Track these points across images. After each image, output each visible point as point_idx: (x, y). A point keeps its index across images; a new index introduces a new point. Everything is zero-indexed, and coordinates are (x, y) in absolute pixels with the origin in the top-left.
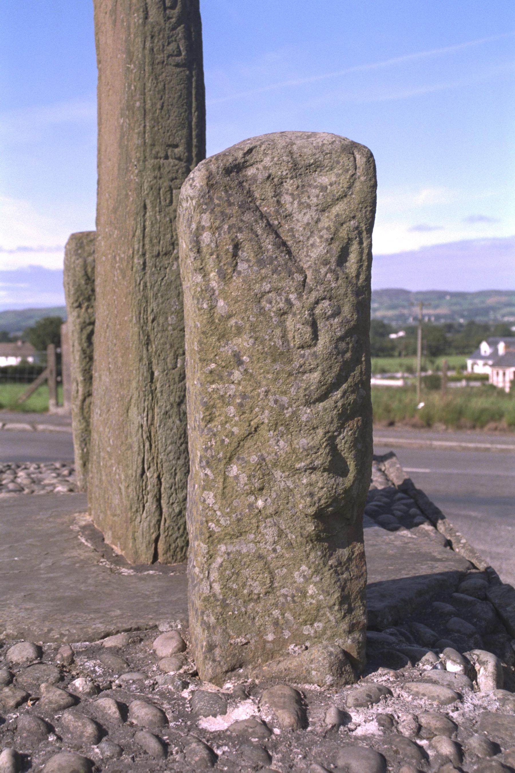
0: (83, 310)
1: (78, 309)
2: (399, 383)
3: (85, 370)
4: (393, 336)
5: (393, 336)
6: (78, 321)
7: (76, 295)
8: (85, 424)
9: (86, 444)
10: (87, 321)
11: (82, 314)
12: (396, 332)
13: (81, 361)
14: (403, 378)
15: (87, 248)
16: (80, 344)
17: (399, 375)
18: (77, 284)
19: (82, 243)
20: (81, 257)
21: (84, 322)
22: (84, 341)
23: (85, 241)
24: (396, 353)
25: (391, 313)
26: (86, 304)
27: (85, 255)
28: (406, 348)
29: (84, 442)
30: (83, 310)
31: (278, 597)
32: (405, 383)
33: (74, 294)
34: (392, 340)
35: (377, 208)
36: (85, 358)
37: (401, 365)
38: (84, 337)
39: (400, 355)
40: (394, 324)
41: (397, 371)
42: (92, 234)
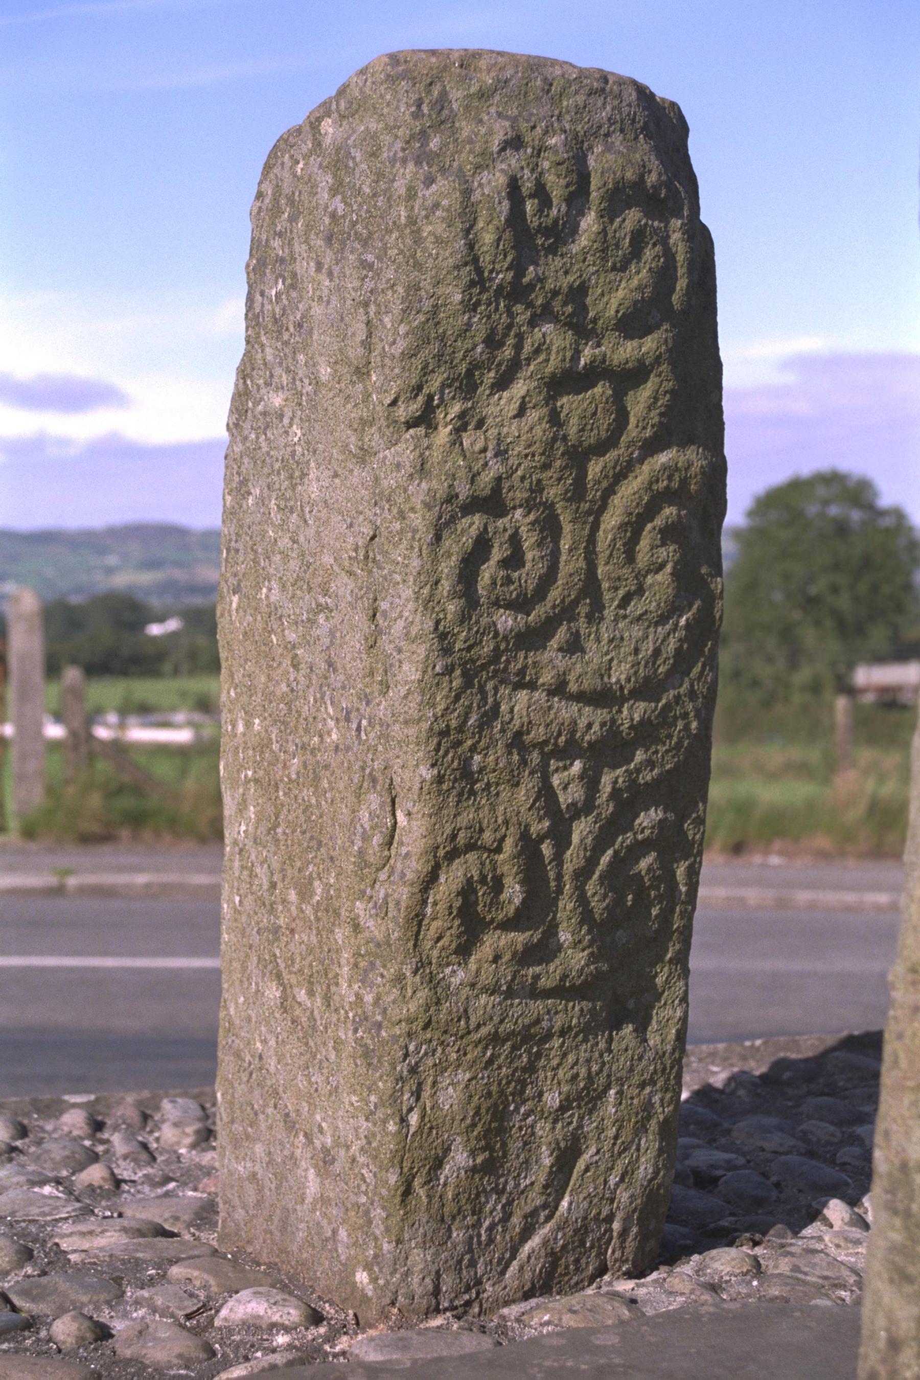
0: (443, 434)
1: (421, 430)
2: (183, 736)
3: (445, 733)
4: (155, 630)
5: (155, 630)
6: (419, 491)
7: (417, 363)
8: (423, 994)
9: (417, 1094)
10: (463, 491)
11: (436, 455)
12: (161, 619)
13: (427, 688)
14: (190, 724)
15: (466, 129)
16: (429, 603)
17: (180, 717)
18: (427, 305)
19: (442, 101)
20: (443, 170)
21: (451, 498)
22: (446, 586)
23: (456, 95)
24: (167, 667)
25: (147, 578)
26: (456, 409)
27: (466, 159)
28: (193, 655)
29: (412, 1084)
30: (443, 434)
31: (90, 1302)
32: (198, 737)
33: (409, 355)
34: (154, 639)
35: (701, 202)
36: (449, 670)
37: (183, 694)
38: (448, 567)
39: (176, 672)
40: (155, 602)
41: (174, 709)
42: (483, 64)
